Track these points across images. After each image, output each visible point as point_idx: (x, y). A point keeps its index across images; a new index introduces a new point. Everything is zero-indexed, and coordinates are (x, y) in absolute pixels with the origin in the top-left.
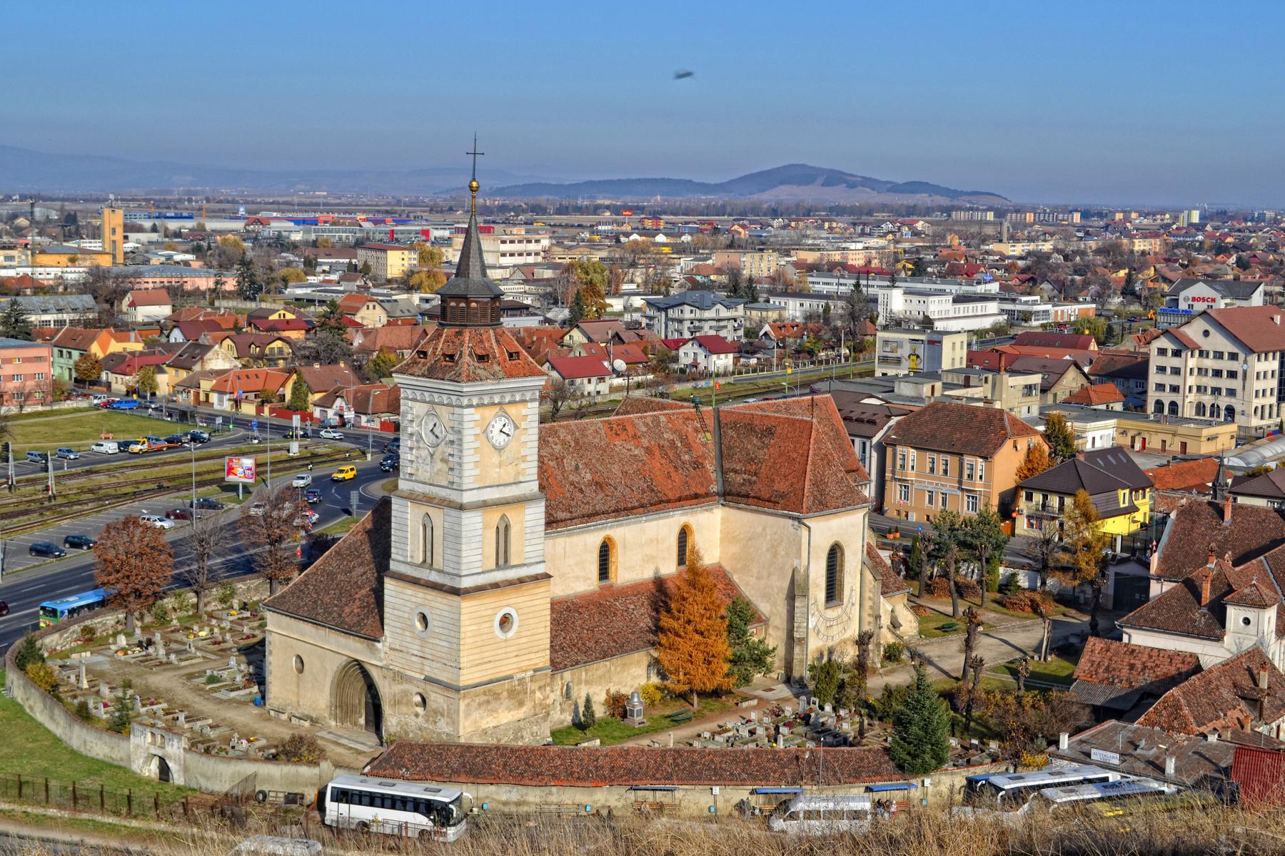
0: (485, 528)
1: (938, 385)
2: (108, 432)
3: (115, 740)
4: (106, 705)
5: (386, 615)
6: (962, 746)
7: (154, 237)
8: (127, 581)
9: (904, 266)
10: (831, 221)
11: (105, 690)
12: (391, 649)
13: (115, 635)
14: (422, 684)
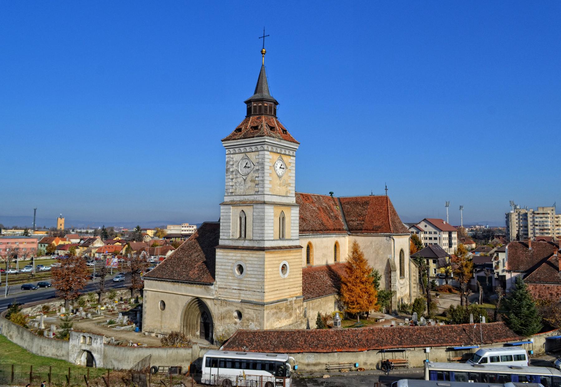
14: (239, 305)
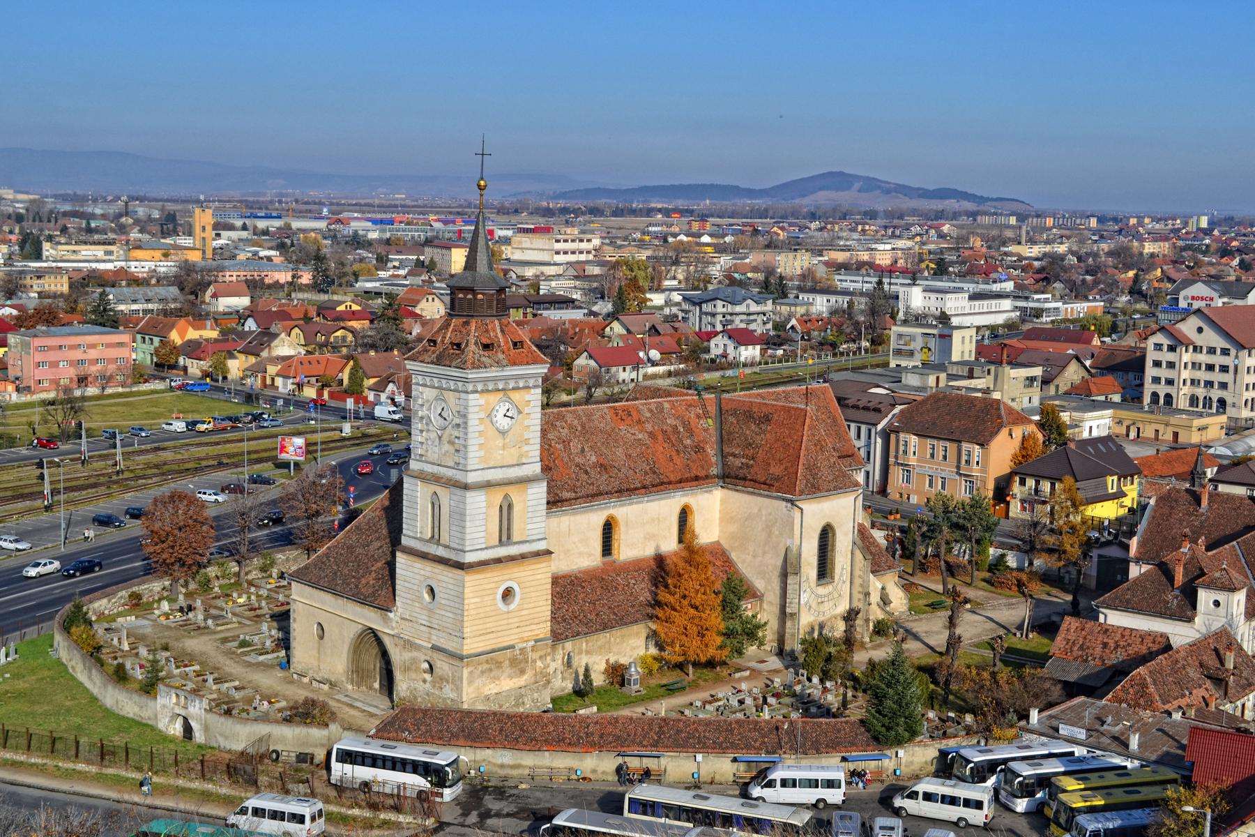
0: (488, 507)
1: (943, 376)
2: (180, 412)
3: (144, 699)
4: (141, 667)
5: (397, 587)
6: (940, 718)
7: (244, 234)
8: (171, 551)
9: (928, 266)
10: (864, 224)
11: (143, 652)
12: (402, 619)
13: (160, 600)
